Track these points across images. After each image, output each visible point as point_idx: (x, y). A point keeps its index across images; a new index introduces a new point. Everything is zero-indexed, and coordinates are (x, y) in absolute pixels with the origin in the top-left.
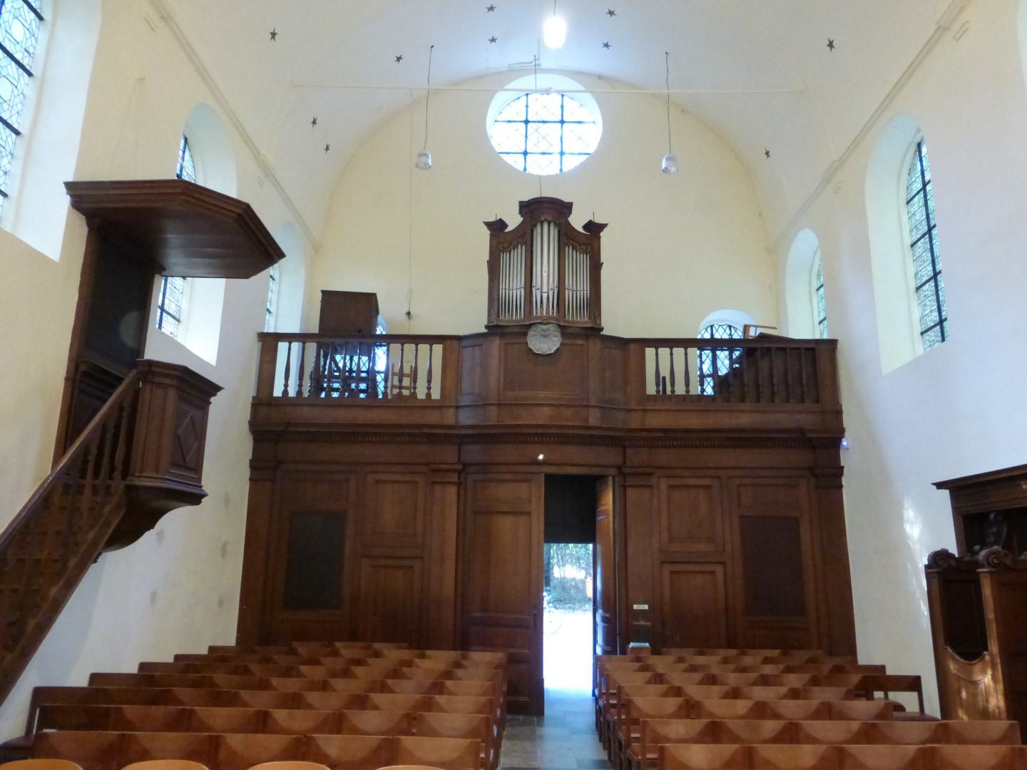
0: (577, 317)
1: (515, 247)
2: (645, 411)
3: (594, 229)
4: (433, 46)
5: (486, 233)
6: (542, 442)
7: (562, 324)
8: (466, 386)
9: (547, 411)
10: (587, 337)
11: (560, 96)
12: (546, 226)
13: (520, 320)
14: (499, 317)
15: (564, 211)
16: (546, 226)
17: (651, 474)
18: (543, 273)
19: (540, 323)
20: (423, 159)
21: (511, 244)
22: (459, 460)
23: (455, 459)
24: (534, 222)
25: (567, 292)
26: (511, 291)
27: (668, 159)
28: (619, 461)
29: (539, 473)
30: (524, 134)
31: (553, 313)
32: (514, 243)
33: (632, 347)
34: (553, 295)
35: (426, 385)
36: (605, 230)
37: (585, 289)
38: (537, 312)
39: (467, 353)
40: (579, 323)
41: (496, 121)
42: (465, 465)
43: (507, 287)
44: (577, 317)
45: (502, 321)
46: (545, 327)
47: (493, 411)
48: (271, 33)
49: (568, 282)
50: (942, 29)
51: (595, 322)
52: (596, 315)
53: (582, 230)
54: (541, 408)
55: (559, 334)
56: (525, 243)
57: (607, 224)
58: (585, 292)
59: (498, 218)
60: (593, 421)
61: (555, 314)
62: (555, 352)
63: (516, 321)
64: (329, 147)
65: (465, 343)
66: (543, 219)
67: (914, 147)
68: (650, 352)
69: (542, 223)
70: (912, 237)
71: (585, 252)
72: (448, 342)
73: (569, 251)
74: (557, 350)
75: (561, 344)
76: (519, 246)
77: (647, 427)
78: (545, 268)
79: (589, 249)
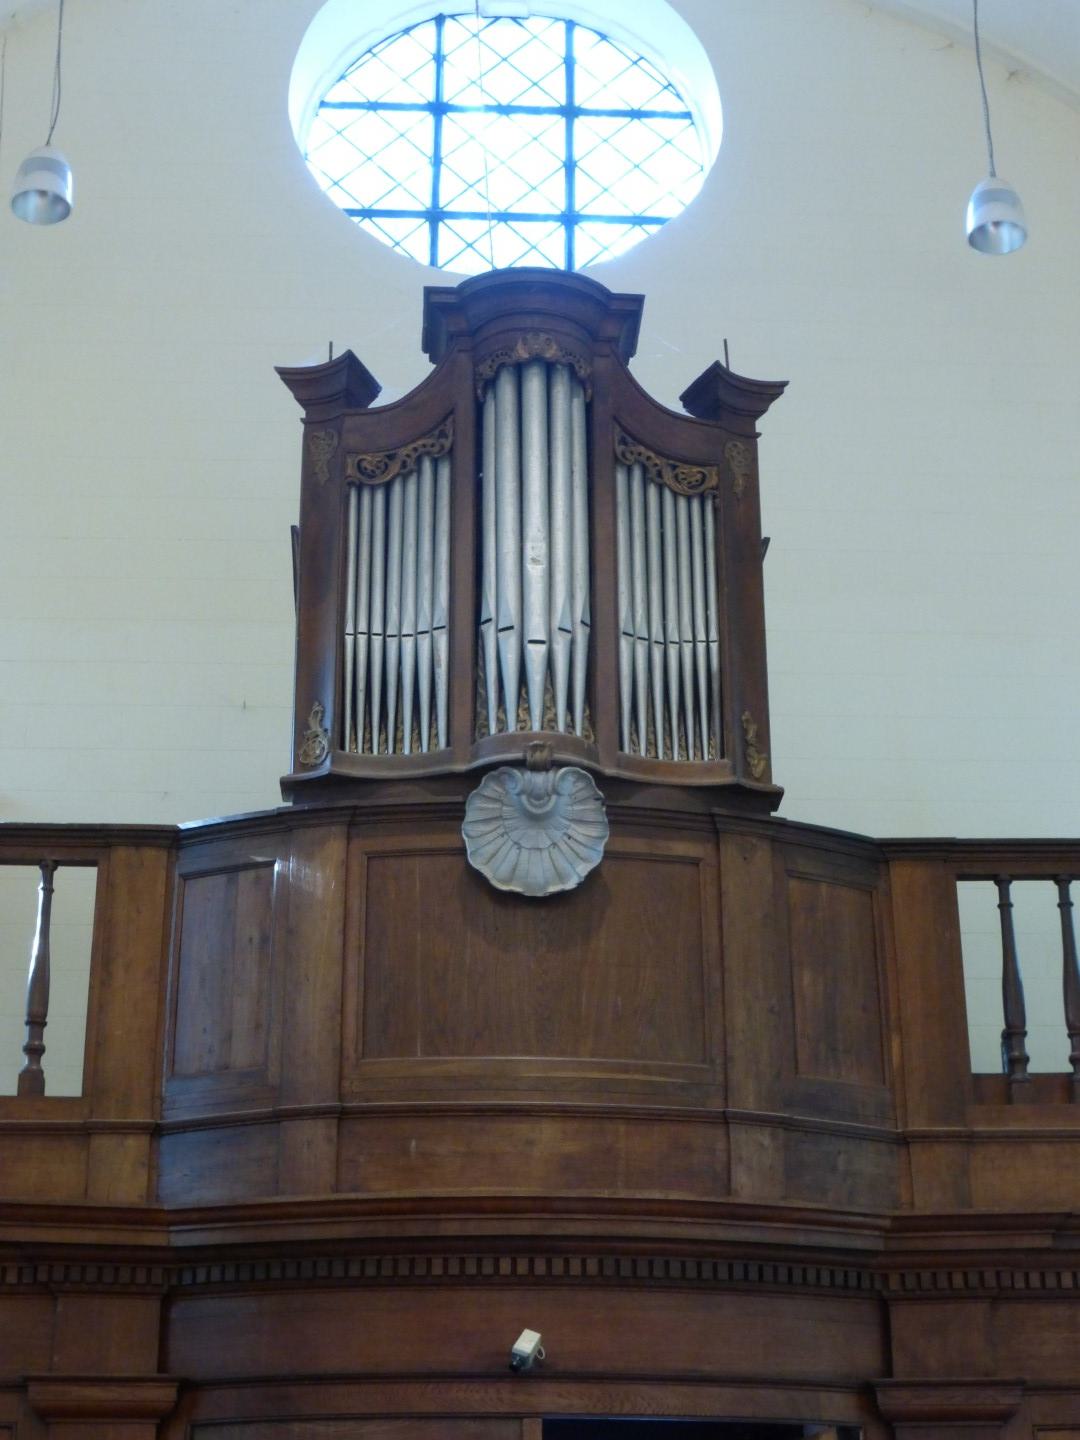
0: (669, 748)
2: (970, 1140)
5: (289, 414)
6: (532, 1282)
7: (610, 771)
8: (196, 1039)
9: (548, 1136)
10: (713, 831)
11: (562, 26)
12: (534, 385)
13: (433, 758)
14: (342, 747)
15: (610, 329)
16: (534, 385)
17: (1004, 1417)
18: (530, 567)
19: (520, 764)
20: (44, 180)
21: (391, 457)
22: (162, 1366)
23: (147, 1365)
24: (486, 370)
25: (624, 644)
26: (392, 644)
27: (988, 197)
28: (864, 1358)
29: (518, 1417)
30: (430, 151)
31: (571, 725)
32: (403, 452)
33: (903, 876)
34: (569, 652)
35: (23, 1035)
36: (775, 407)
37: (701, 636)
38: (502, 723)
39: (203, 900)
40: (671, 767)
41: (323, 104)
42: (188, 1387)
43: (377, 627)
44: (669, 748)
45: (353, 761)
46: (539, 779)
47: (313, 1142)
49: (631, 608)
51: (747, 766)
52: (751, 735)
53: (678, 408)
54: (524, 1128)
55: (593, 810)
57: (783, 384)
58: (701, 647)
59: (338, 354)
60: (748, 1187)
61: (578, 732)
62: (580, 885)
63: (410, 762)
65: (190, 861)
66: (522, 353)
68: (975, 899)
69: (519, 371)
71: (698, 492)
72: (121, 854)
73: (628, 487)
74: (593, 875)
75: (608, 855)
76: (427, 466)
77: (981, 1208)
78: (535, 547)
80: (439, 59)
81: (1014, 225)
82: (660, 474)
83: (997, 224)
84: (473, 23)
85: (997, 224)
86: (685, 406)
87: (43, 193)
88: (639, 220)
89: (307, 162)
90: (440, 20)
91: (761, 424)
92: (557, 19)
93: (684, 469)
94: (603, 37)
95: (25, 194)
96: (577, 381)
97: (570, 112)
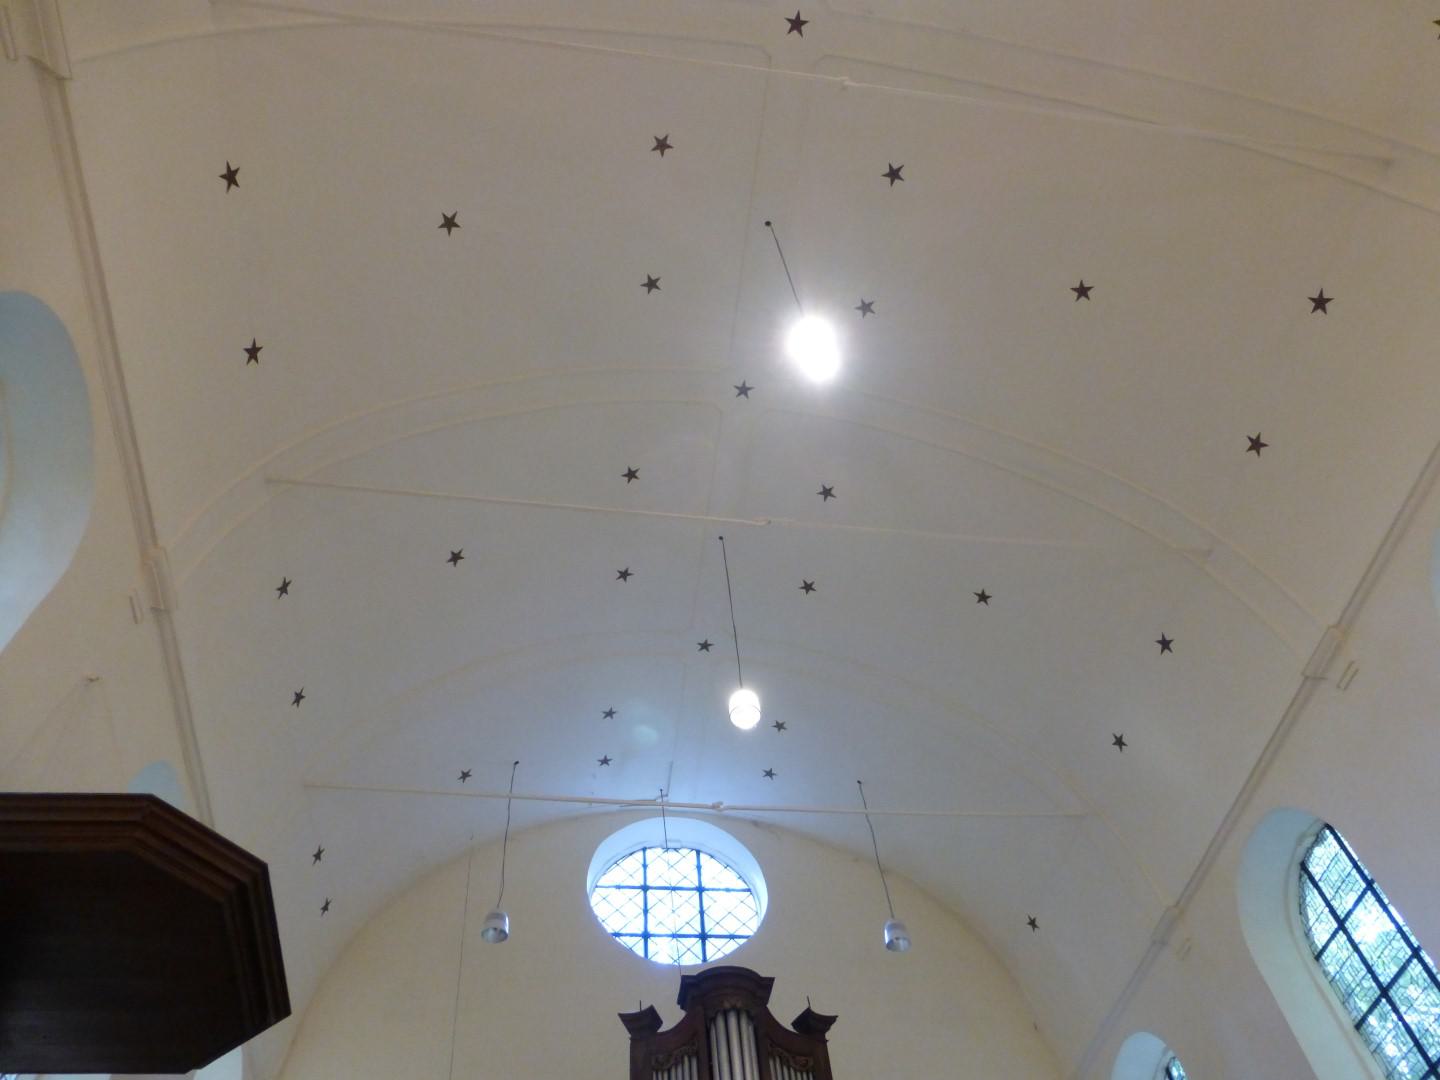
1: (679, 1062)
3: (814, 1026)
4: (517, 763)
5: (624, 1037)
11: (694, 853)
12: (733, 1021)
16: (733, 1021)
20: (496, 923)
27: (892, 928)
36: (833, 1027)
48: (296, 694)
50: (1313, 679)
56: (697, 1054)
59: (645, 1007)
64: (330, 907)
66: (727, 1005)
67: (1296, 869)
70: (1350, 1013)
73: (775, 1067)
76: (686, 1059)
79: (811, 1063)
80: (645, 866)
81: (904, 939)
82: (788, 1061)
83: (897, 939)
84: (659, 851)
85: (897, 939)
86: (795, 1028)
87: (495, 929)
88: (732, 937)
89: (1371, 1036)
90: (644, 849)
91: (828, 1035)
92: (693, 850)
93: (798, 1058)
94: (712, 857)
95: (487, 930)
96: (751, 1018)
97: (645, 888)
